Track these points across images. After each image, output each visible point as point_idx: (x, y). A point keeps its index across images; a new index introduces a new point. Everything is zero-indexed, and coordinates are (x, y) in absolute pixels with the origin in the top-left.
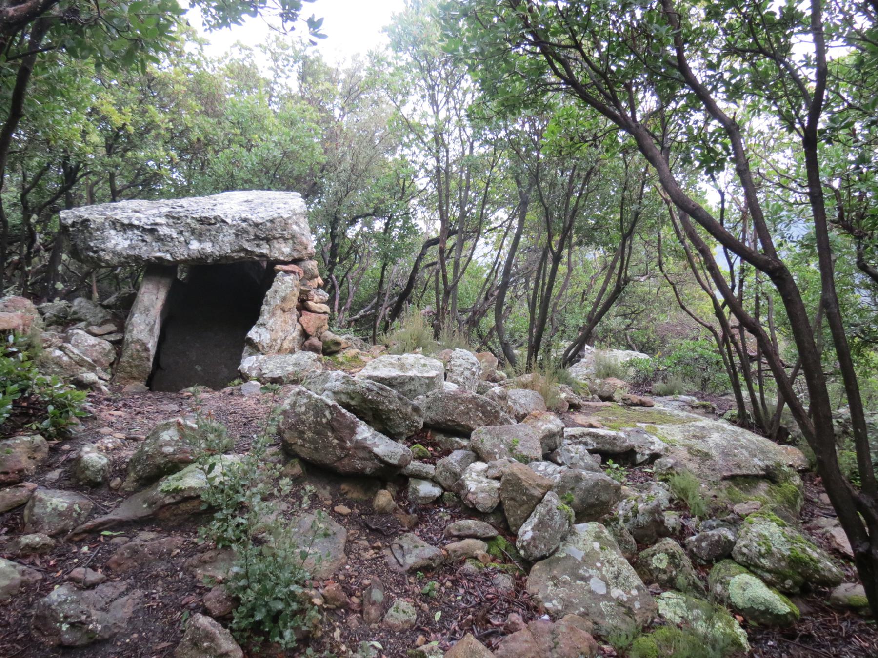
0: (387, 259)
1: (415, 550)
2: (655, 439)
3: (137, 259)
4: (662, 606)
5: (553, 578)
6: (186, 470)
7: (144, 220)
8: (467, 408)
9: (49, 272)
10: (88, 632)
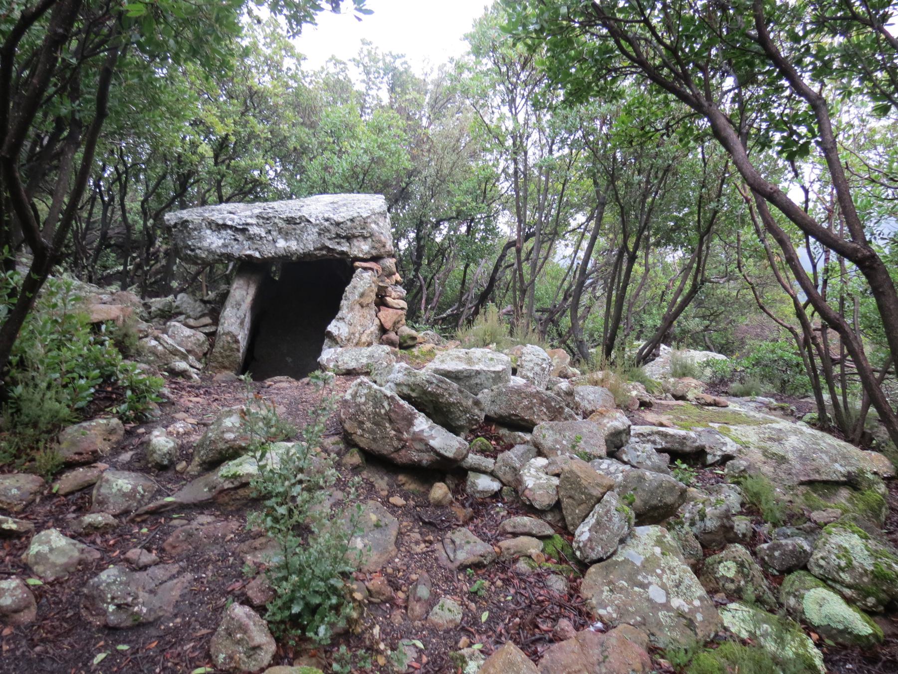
0: (470, 259)
1: (467, 545)
2: (727, 440)
3: (229, 257)
4: (727, 618)
5: (610, 583)
6: (245, 457)
7: (237, 220)
8: (531, 402)
9: (167, 273)
10: (133, 614)
